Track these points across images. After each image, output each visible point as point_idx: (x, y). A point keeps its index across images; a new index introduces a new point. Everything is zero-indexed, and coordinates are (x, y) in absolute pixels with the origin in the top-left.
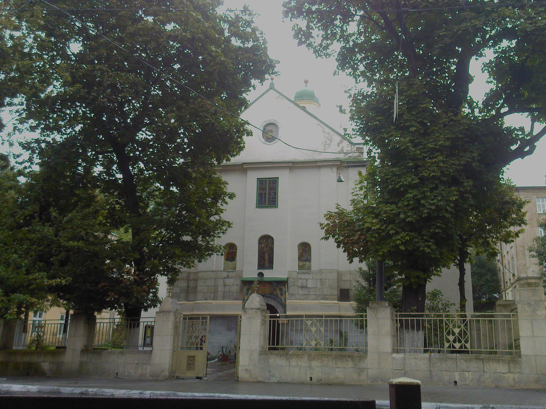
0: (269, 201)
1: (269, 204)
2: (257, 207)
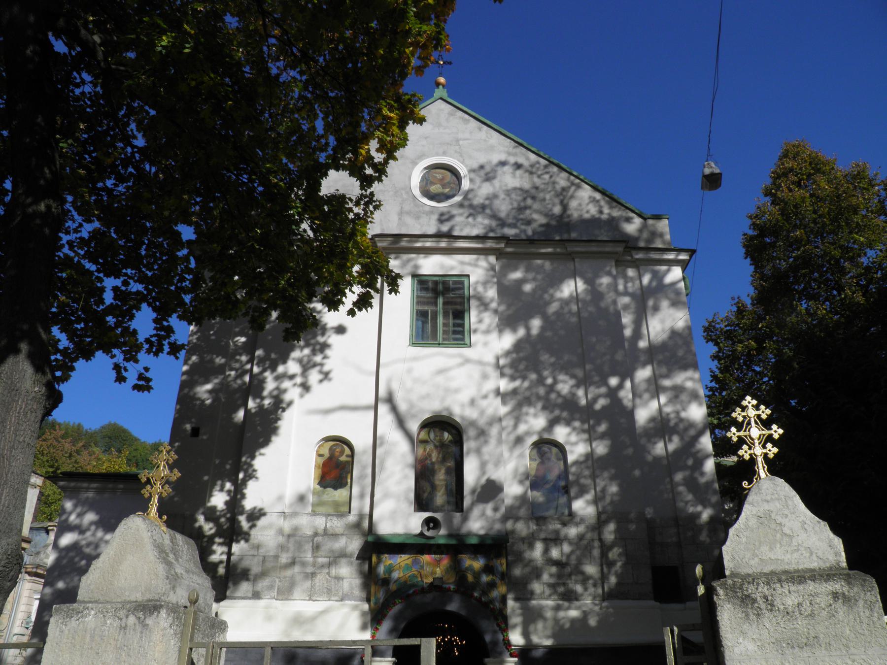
0: (444, 332)
1: (444, 339)
2: (413, 344)
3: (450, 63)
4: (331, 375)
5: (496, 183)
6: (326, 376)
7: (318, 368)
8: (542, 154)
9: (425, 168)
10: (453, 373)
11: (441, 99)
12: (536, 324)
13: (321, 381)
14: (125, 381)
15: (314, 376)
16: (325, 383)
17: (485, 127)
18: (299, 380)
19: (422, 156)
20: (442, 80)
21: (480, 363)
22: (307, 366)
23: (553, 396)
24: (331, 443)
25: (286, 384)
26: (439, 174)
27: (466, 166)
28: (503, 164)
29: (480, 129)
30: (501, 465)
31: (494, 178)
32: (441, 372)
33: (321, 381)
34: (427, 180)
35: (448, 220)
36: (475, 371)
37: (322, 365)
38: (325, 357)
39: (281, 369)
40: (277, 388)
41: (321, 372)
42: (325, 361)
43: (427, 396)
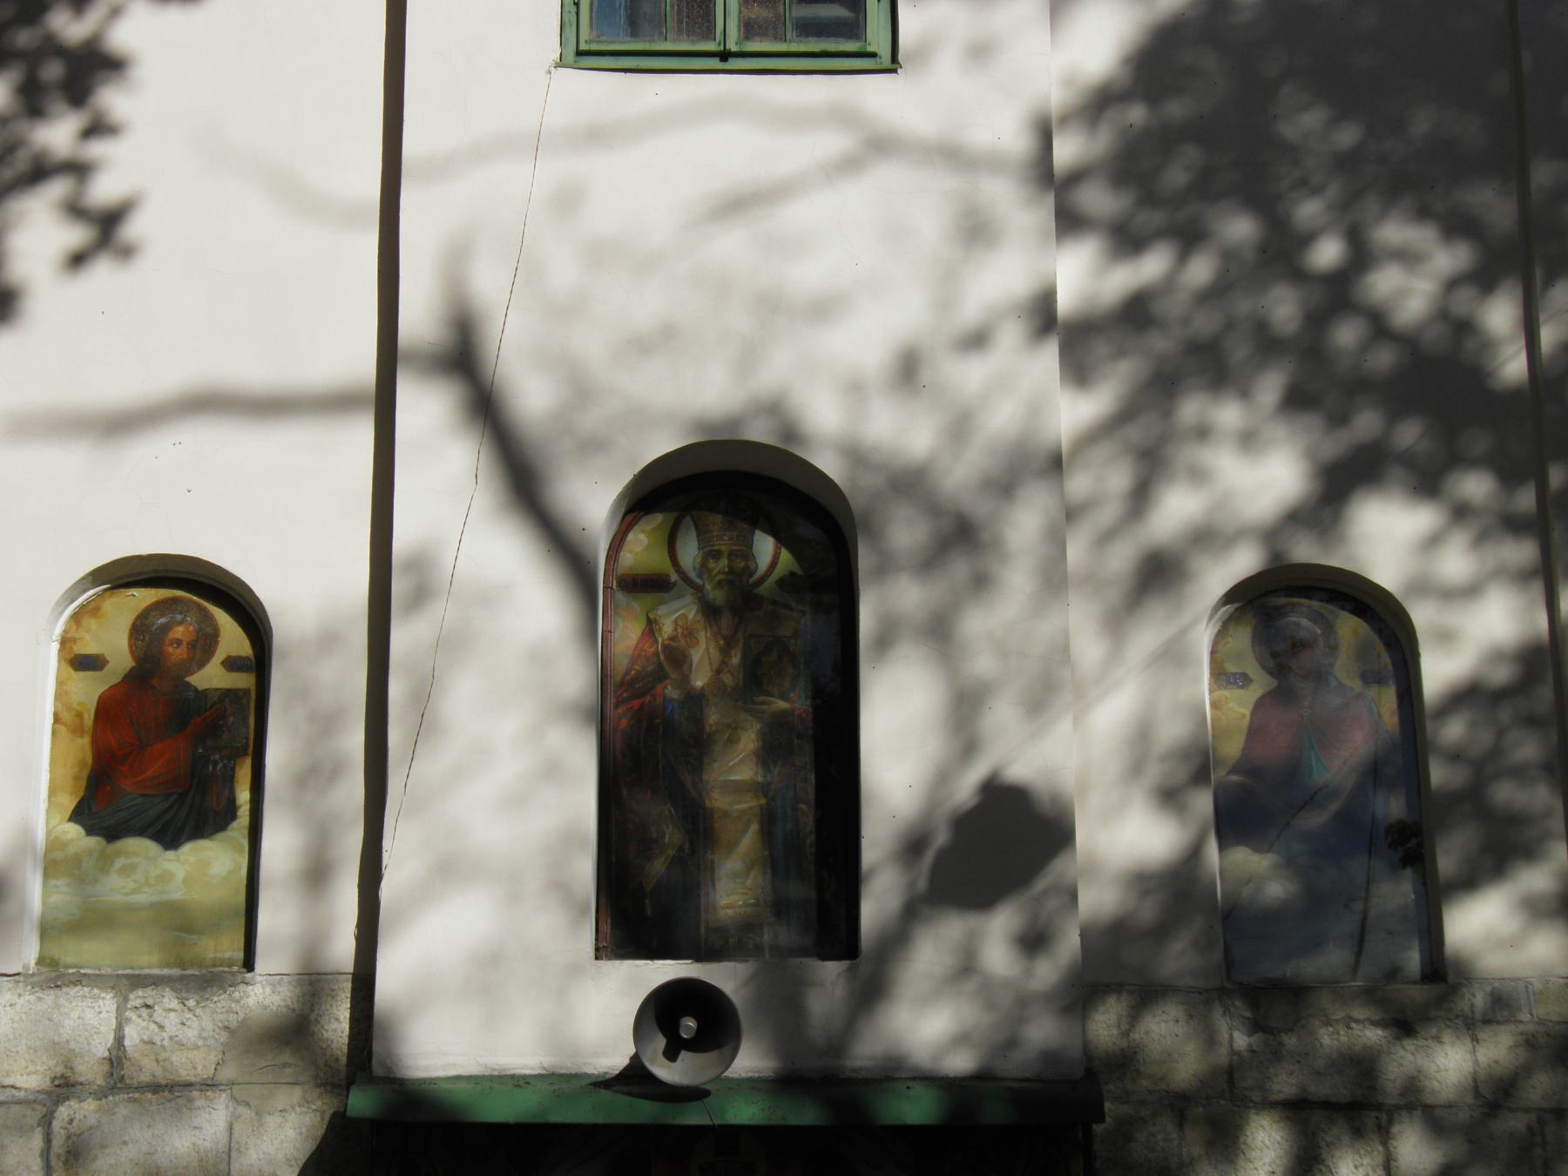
2: (582, 56)
6: (105, 231)
7: (57, 189)
10: (799, 214)
13: (77, 260)
16: (102, 272)
21: (951, 155)
24: (144, 597)
32: (738, 204)
33: (77, 260)
37: (79, 170)
38: (98, 128)
41: (75, 210)
42: (97, 149)
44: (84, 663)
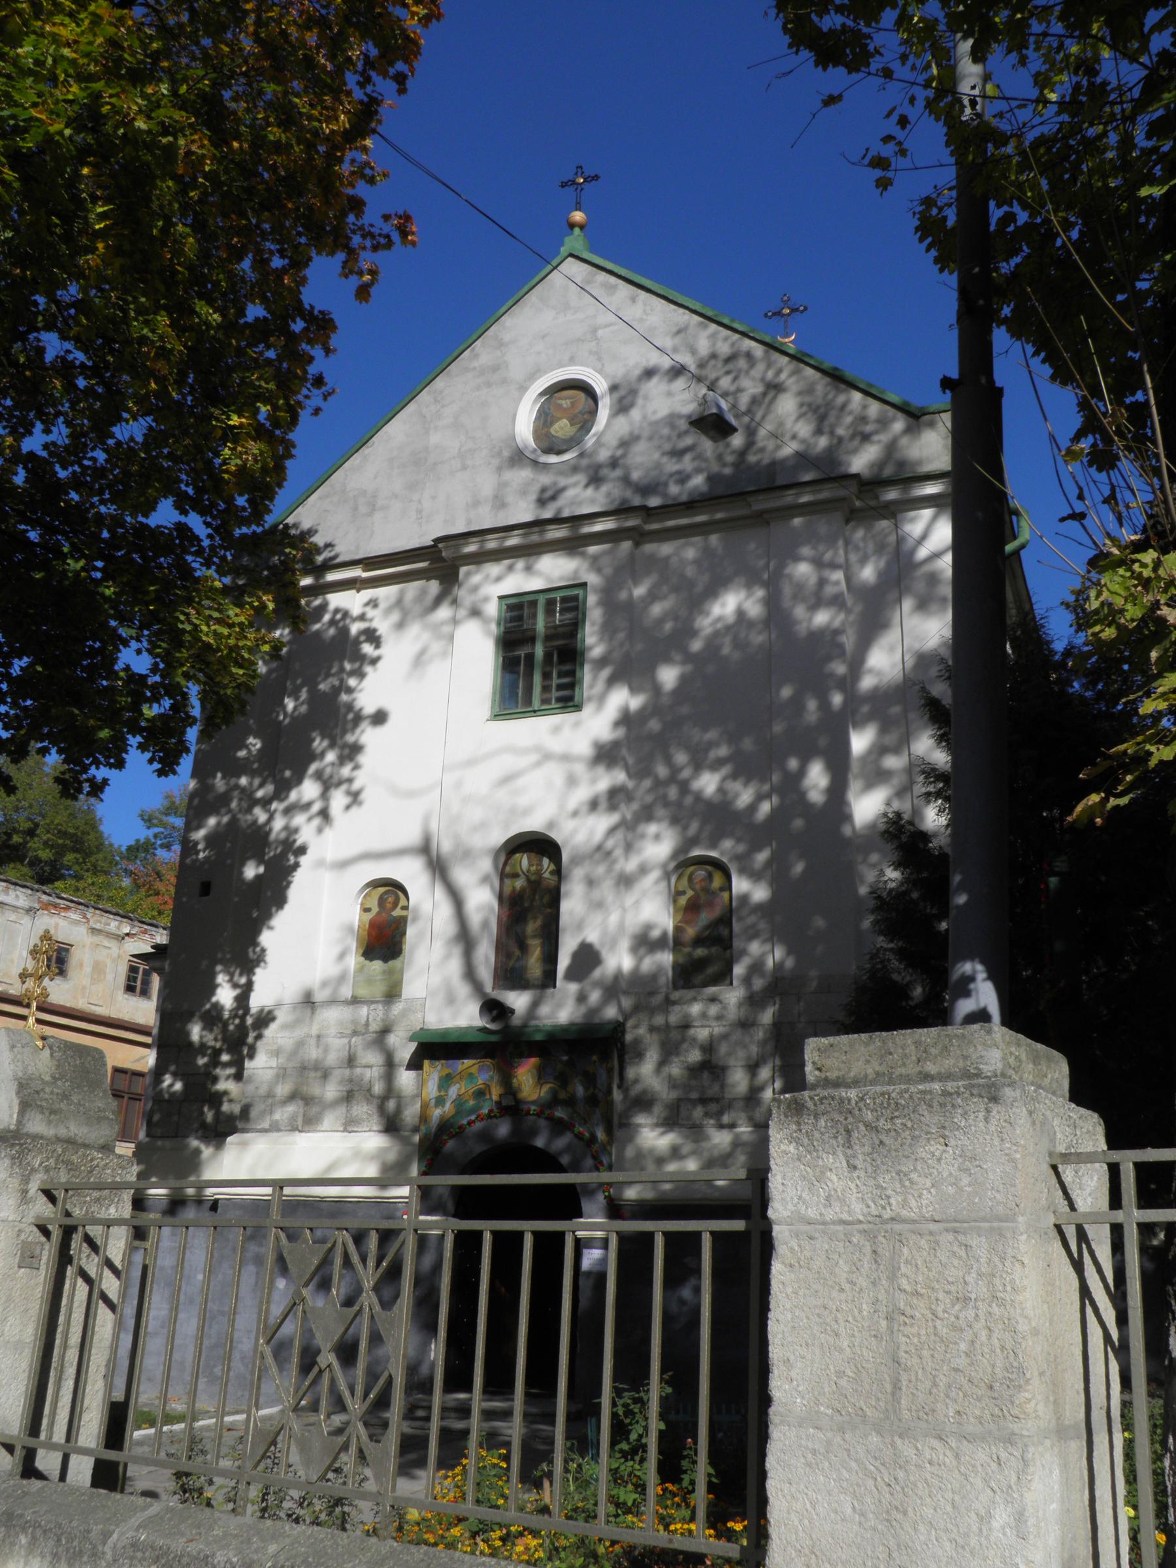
2: (496, 716)
3: (596, 178)
4: (363, 796)
5: (636, 414)
6: (355, 798)
7: (344, 787)
8: (736, 325)
9: (542, 394)
10: (520, 782)
11: (571, 255)
12: (668, 676)
13: (348, 807)
14: (161, 773)
15: (338, 799)
16: (354, 810)
17: (643, 295)
18: (316, 807)
19: (533, 376)
20: (578, 216)
21: (566, 758)
22: (328, 784)
23: (688, 800)
24: (382, 890)
25: (299, 820)
26: (565, 400)
27: (605, 377)
28: (649, 373)
29: (633, 300)
30: (621, 916)
31: (632, 405)
32: (507, 779)
33: (348, 807)
34: (547, 415)
35: (553, 498)
36: (555, 773)
37: (350, 780)
38: (357, 767)
39: (293, 796)
40: (286, 828)
41: (348, 793)
42: (355, 773)
43: (483, 826)
44: (367, 910)
